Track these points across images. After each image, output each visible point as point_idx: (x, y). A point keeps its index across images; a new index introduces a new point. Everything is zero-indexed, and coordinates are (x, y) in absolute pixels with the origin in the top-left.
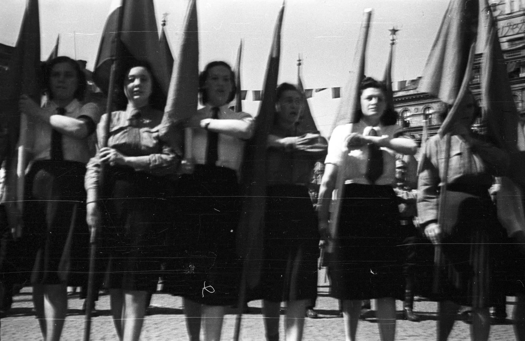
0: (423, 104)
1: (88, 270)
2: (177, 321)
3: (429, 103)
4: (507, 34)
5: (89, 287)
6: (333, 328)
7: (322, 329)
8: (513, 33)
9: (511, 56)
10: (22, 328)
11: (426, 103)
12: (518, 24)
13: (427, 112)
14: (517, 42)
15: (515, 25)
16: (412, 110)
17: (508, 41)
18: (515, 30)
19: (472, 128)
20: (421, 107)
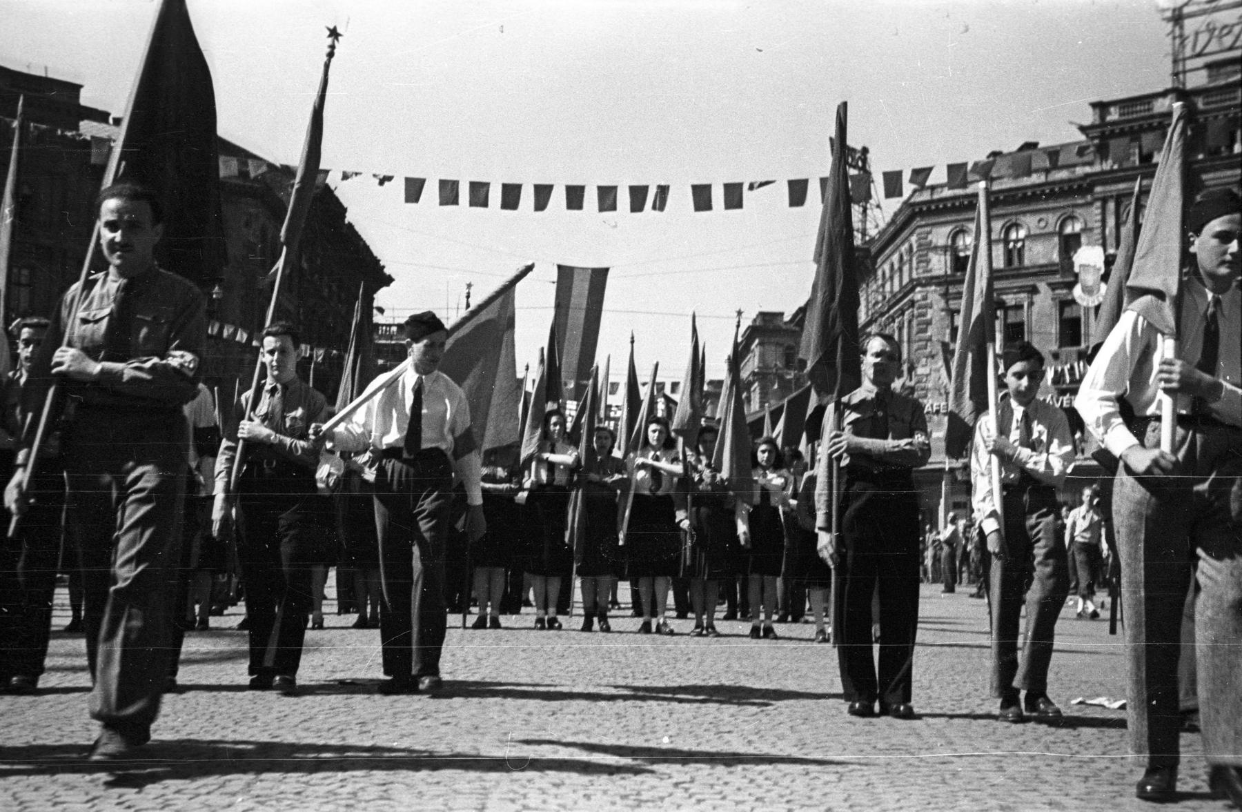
0: (952, 222)
1: (418, 650)
2: (414, 716)
3: (1017, 214)
4: (1207, 51)
5: (617, 758)
6: (781, 737)
7: (754, 738)
8: (1217, 50)
9: (1221, 101)
10: (47, 730)
11: (1011, 214)
12: (1233, 25)
13: (1068, 230)
14: (1230, 68)
15: (1225, 27)
16: (1031, 222)
17: (1209, 66)
18: (1225, 39)
19: (54, 371)
20: (1052, 219)
